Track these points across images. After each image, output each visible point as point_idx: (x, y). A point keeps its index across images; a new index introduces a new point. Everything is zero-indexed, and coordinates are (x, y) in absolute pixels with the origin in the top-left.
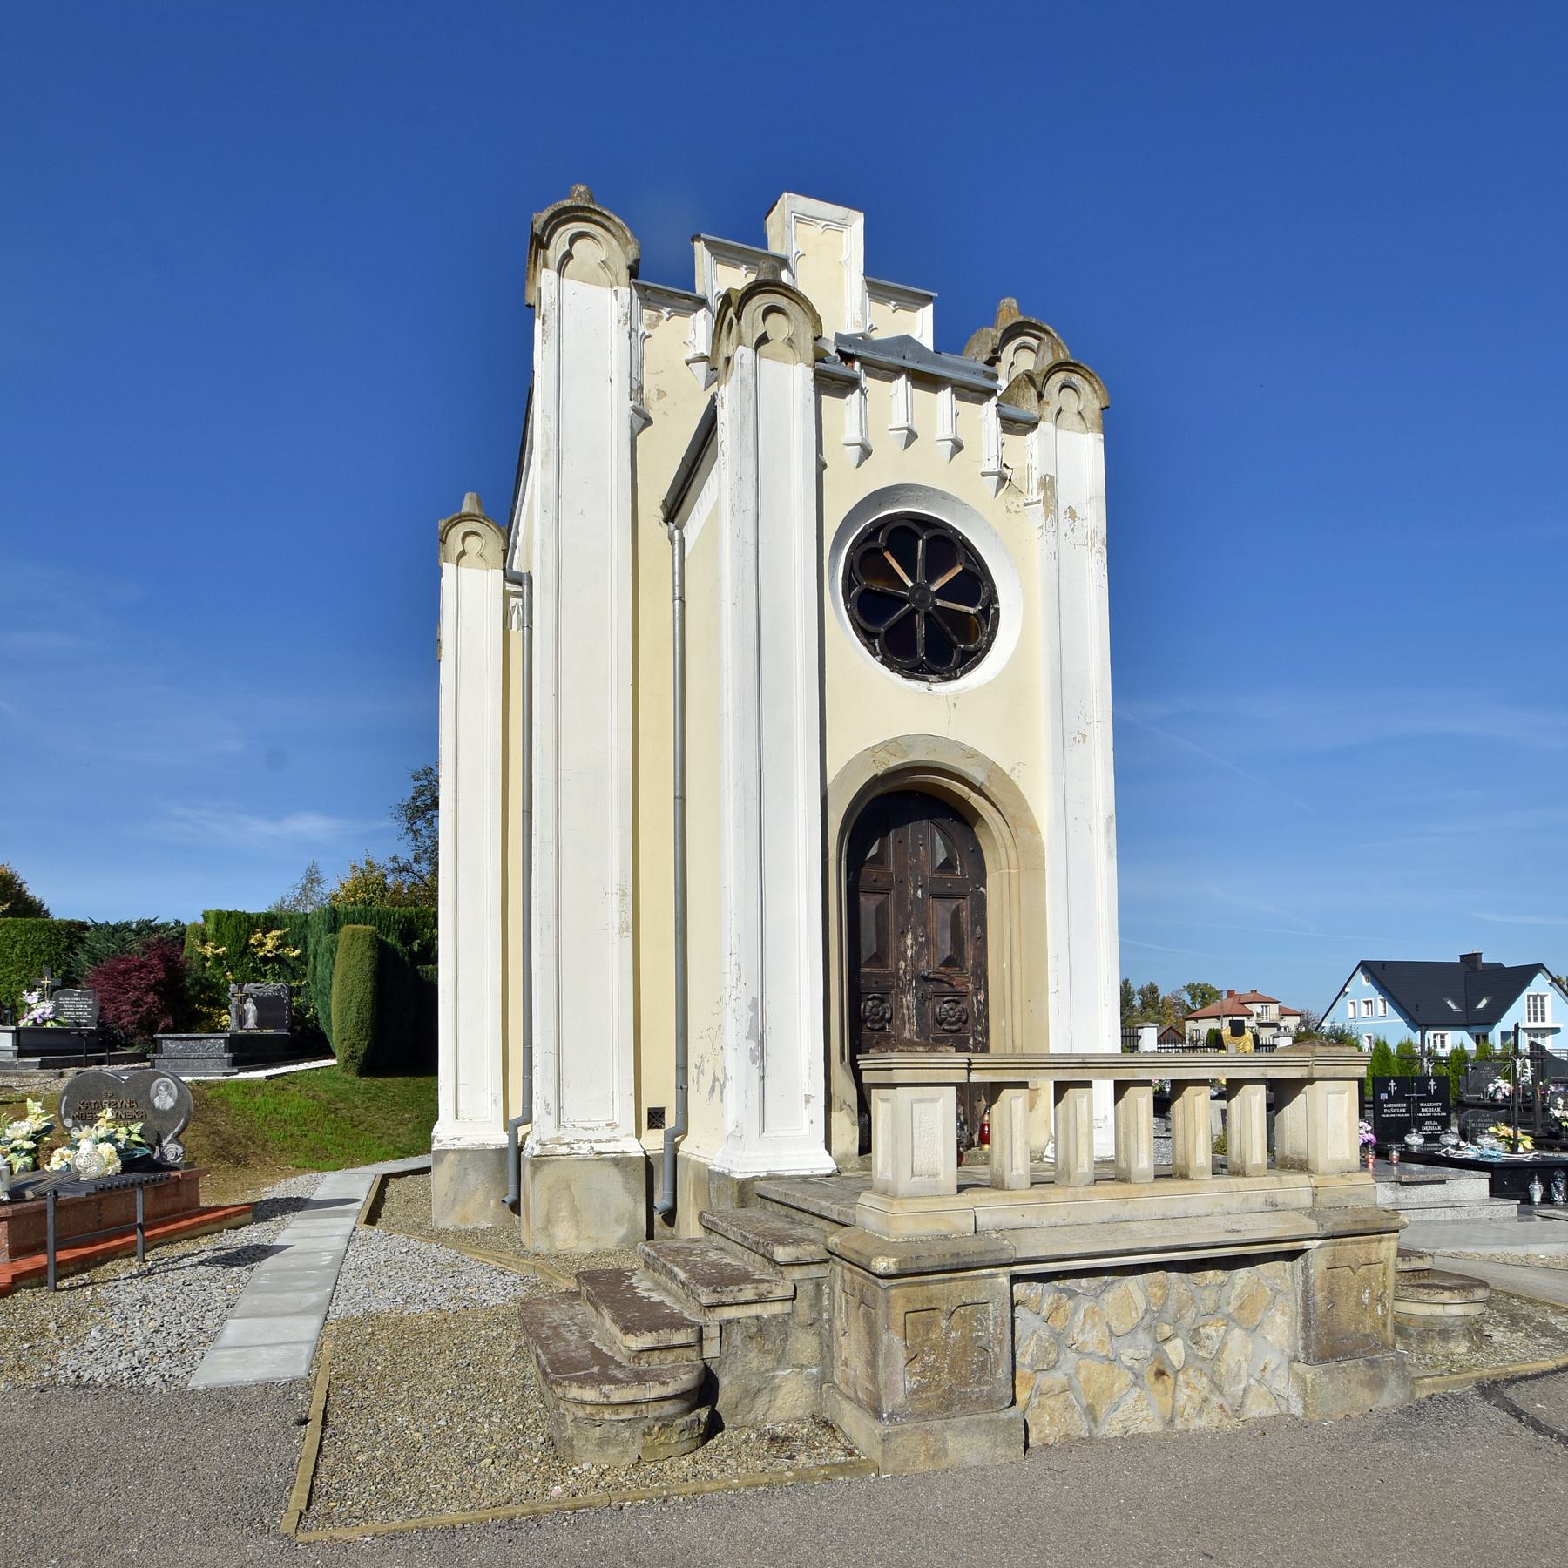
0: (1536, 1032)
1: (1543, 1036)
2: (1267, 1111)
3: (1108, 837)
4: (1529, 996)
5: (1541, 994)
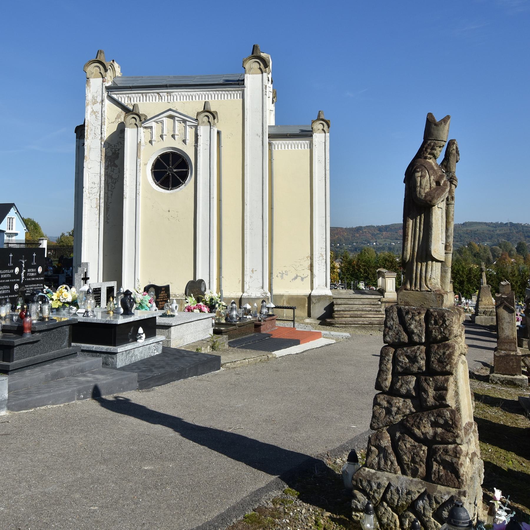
0: (9, 235)
1: (12, 236)
2: (244, 79)
3: (266, 115)
4: (8, 218)
5: (12, 217)
